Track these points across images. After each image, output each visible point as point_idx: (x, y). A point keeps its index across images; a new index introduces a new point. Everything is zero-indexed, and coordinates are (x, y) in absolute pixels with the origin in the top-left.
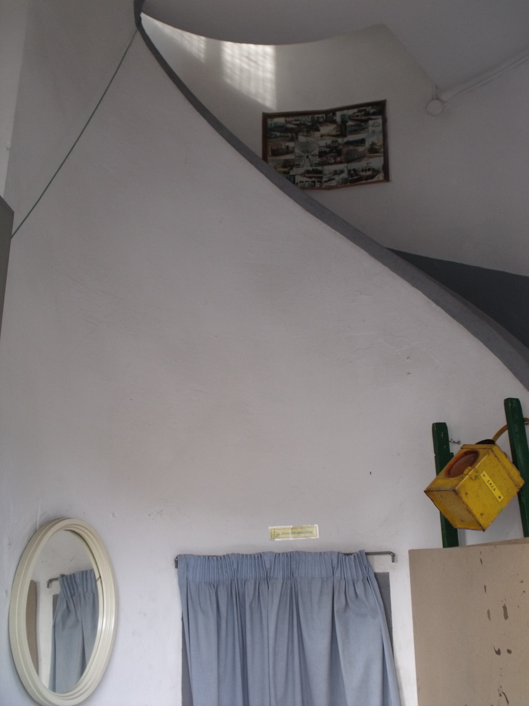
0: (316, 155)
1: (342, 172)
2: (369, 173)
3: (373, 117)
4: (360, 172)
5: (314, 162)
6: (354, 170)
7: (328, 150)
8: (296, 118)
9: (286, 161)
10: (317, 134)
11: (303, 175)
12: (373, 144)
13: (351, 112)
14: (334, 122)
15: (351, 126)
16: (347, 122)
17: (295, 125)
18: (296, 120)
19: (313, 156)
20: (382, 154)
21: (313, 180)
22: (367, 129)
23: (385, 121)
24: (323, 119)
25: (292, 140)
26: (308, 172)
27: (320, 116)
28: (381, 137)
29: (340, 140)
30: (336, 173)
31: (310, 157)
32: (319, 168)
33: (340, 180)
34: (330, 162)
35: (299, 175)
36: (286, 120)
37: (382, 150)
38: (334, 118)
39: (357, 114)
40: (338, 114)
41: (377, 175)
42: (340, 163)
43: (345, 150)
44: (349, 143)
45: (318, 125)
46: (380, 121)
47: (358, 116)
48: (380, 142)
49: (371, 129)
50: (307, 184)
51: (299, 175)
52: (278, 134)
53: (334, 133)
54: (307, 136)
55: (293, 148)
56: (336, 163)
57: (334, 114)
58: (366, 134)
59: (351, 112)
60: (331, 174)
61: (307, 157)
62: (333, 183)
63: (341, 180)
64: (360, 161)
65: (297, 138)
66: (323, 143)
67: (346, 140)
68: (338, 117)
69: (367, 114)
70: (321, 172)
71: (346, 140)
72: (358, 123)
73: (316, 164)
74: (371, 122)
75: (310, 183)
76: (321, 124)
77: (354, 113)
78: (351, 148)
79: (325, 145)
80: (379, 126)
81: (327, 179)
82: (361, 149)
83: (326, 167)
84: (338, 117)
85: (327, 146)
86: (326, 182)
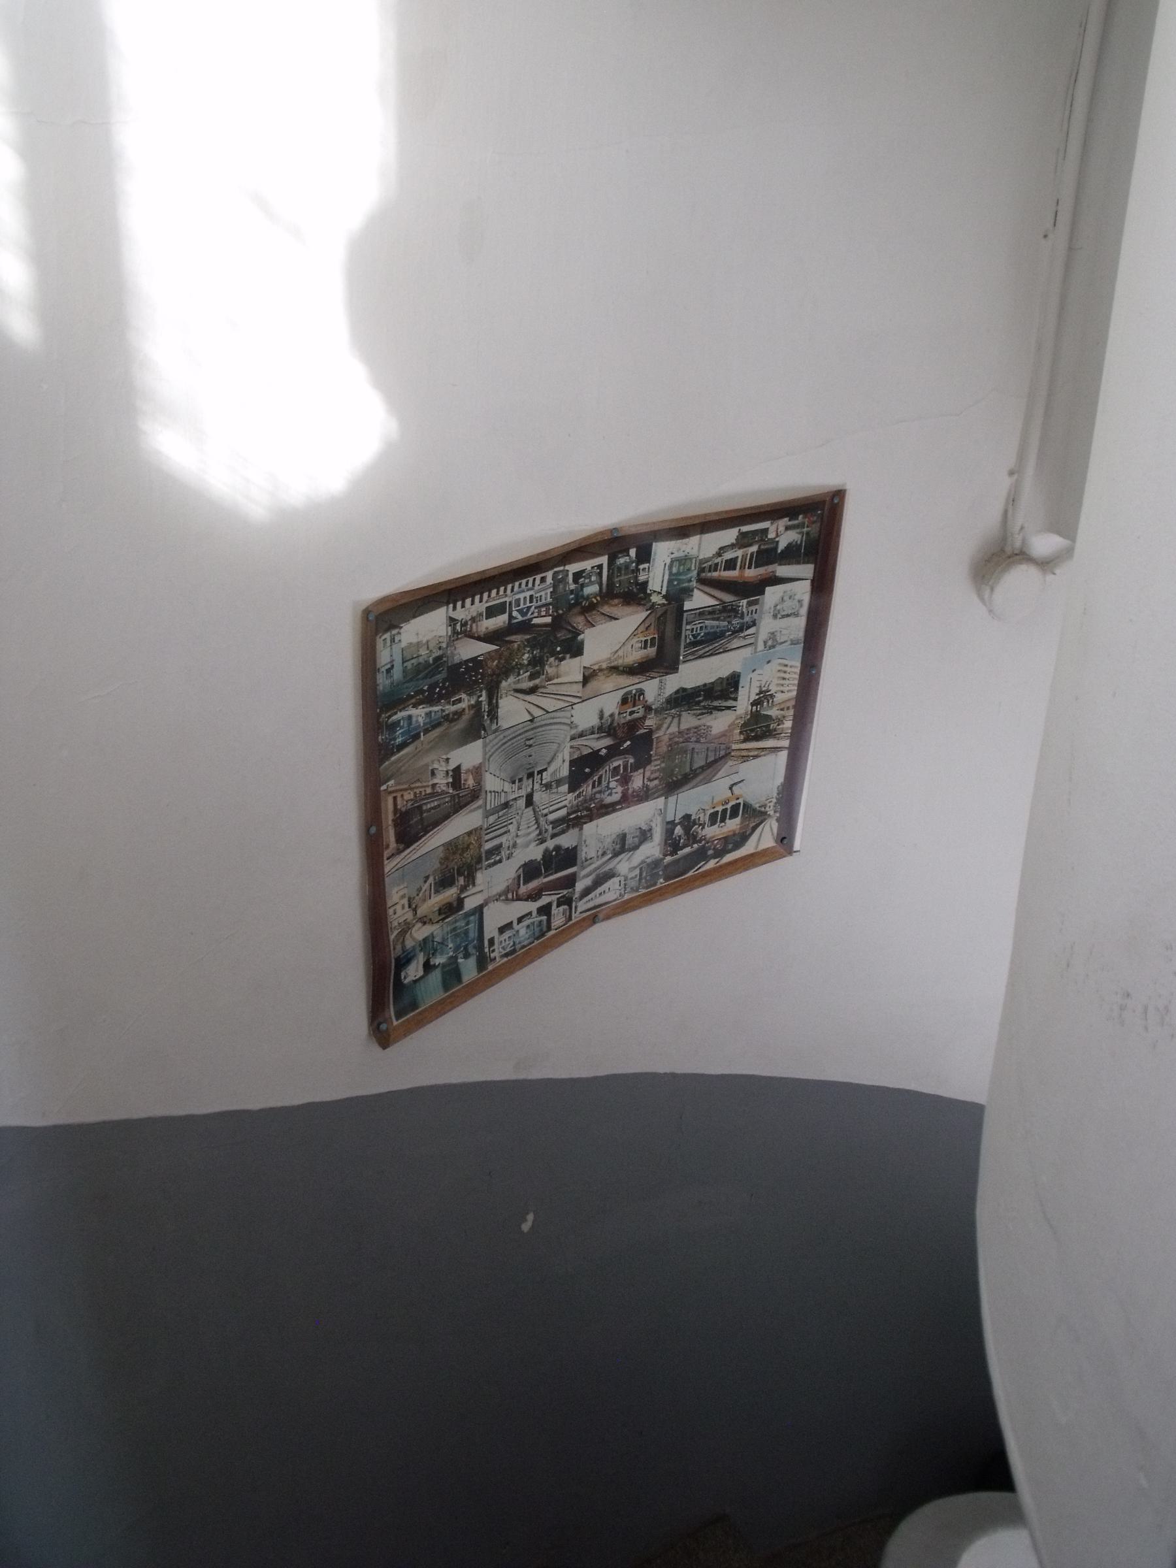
0: (559, 782)
1: (645, 835)
2: (733, 825)
3: (782, 571)
4: (703, 826)
5: (552, 817)
6: (688, 821)
7: (601, 744)
8: (494, 597)
9: (453, 848)
10: (571, 669)
11: (510, 894)
12: (764, 697)
13: (706, 546)
14: (636, 595)
15: (702, 613)
16: (688, 592)
17: (488, 638)
18: (492, 612)
19: (548, 786)
20: (786, 743)
21: (544, 901)
22: (752, 630)
23: (823, 585)
24: (601, 585)
25: (475, 729)
26: (530, 871)
27: (587, 565)
28: (795, 664)
29: (654, 689)
30: (622, 846)
31: (539, 797)
32: (567, 840)
33: (632, 875)
34: (609, 800)
35: (497, 898)
36: (452, 621)
37: (788, 724)
38: (642, 578)
39: (729, 555)
40: (663, 552)
41: (754, 829)
42: (644, 795)
43: (666, 730)
44: (685, 699)
45: (579, 621)
46: (802, 590)
47: (731, 565)
48: (787, 692)
49: (767, 625)
50: (522, 931)
51: (497, 898)
52: (419, 714)
53: (635, 655)
54: (532, 691)
55: (478, 771)
56: (627, 800)
57: (645, 555)
58: (747, 652)
59: (706, 546)
60: (604, 854)
61: (529, 801)
62: (611, 892)
63: (637, 872)
64: (708, 781)
65: (493, 714)
66: (586, 716)
67: (674, 683)
68: (656, 577)
69: (768, 556)
70: (569, 857)
71: (674, 683)
72: (728, 598)
73: (555, 823)
74: (772, 594)
75: (536, 919)
76: (588, 608)
77: (722, 550)
78: (689, 720)
79: (594, 721)
80: (796, 615)
81: (588, 882)
82: (720, 723)
83: (589, 828)
84: (656, 577)
85: (606, 728)
86: (587, 892)
